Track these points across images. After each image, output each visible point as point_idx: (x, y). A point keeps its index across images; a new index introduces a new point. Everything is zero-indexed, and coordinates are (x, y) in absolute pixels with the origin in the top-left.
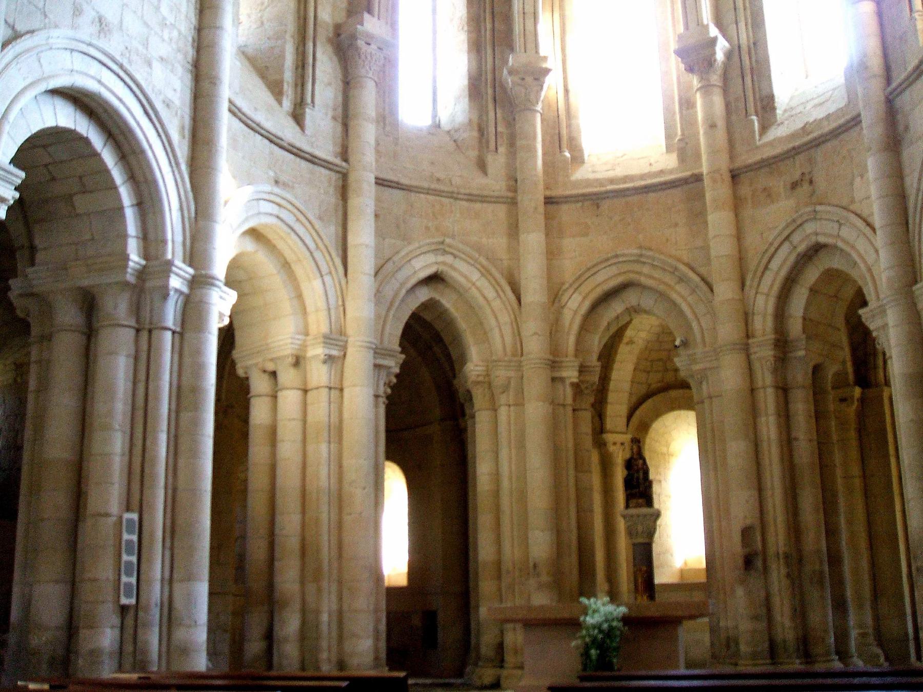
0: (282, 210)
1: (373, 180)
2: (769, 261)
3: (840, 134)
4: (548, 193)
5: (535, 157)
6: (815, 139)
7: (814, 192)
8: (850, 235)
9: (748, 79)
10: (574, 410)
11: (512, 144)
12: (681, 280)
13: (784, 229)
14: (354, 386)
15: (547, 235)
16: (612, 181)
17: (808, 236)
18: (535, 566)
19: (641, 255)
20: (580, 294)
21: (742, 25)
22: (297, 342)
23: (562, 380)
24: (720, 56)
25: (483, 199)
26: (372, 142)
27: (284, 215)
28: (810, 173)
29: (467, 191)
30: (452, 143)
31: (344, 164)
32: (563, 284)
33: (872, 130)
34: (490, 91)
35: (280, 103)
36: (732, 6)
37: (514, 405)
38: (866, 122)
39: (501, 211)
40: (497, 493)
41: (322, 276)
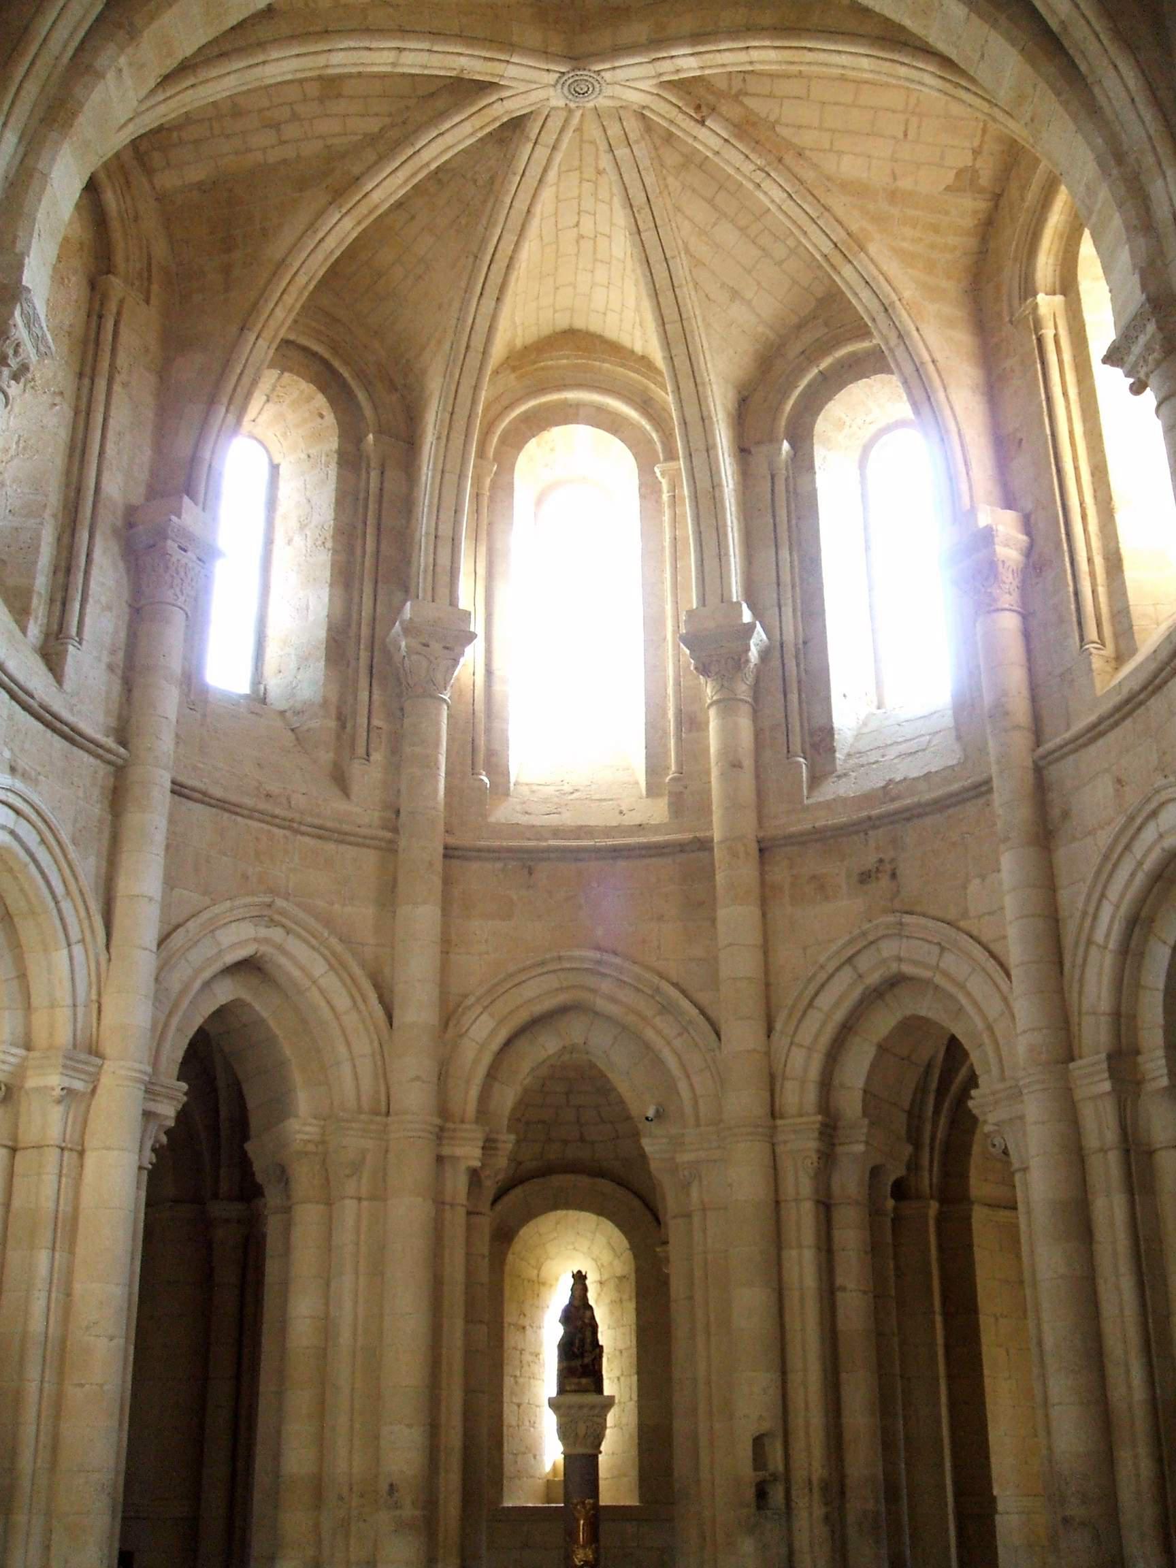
0: (22, 821)
1: (168, 785)
2: (817, 994)
3: (948, 807)
4: (452, 841)
5: (435, 776)
6: (907, 809)
7: (898, 891)
8: (962, 970)
9: (794, 697)
10: (469, 1213)
11: (395, 749)
12: (666, 1008)
13: (844, 946)
14: (108, 1148)
15: (444, 910)
16: (556, 832)
17: (884, 961)
18: (392, 1488)
19: (599, 962)
20: (492, 1016)
21: (788, 611)
22: (12, 1060)
23: (455, 1159)
24: (754, 654)
25: (342, 837)
26: (173, 717)
27: (24, 829)
28: (892, 860)
29: (317, 821)
30: (290, 733)
31: (122, 750)
32: (466, 996)
33: (1008, 806)
34: (364, 655)
35: (24, 630)
36: (774, 579)
37: (366, 1199)
38: (1000, 797)
39: (370, 858)
40: (323, 1354)
41: (69, 945)
